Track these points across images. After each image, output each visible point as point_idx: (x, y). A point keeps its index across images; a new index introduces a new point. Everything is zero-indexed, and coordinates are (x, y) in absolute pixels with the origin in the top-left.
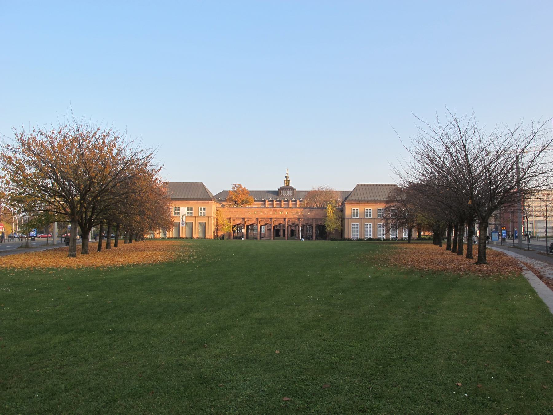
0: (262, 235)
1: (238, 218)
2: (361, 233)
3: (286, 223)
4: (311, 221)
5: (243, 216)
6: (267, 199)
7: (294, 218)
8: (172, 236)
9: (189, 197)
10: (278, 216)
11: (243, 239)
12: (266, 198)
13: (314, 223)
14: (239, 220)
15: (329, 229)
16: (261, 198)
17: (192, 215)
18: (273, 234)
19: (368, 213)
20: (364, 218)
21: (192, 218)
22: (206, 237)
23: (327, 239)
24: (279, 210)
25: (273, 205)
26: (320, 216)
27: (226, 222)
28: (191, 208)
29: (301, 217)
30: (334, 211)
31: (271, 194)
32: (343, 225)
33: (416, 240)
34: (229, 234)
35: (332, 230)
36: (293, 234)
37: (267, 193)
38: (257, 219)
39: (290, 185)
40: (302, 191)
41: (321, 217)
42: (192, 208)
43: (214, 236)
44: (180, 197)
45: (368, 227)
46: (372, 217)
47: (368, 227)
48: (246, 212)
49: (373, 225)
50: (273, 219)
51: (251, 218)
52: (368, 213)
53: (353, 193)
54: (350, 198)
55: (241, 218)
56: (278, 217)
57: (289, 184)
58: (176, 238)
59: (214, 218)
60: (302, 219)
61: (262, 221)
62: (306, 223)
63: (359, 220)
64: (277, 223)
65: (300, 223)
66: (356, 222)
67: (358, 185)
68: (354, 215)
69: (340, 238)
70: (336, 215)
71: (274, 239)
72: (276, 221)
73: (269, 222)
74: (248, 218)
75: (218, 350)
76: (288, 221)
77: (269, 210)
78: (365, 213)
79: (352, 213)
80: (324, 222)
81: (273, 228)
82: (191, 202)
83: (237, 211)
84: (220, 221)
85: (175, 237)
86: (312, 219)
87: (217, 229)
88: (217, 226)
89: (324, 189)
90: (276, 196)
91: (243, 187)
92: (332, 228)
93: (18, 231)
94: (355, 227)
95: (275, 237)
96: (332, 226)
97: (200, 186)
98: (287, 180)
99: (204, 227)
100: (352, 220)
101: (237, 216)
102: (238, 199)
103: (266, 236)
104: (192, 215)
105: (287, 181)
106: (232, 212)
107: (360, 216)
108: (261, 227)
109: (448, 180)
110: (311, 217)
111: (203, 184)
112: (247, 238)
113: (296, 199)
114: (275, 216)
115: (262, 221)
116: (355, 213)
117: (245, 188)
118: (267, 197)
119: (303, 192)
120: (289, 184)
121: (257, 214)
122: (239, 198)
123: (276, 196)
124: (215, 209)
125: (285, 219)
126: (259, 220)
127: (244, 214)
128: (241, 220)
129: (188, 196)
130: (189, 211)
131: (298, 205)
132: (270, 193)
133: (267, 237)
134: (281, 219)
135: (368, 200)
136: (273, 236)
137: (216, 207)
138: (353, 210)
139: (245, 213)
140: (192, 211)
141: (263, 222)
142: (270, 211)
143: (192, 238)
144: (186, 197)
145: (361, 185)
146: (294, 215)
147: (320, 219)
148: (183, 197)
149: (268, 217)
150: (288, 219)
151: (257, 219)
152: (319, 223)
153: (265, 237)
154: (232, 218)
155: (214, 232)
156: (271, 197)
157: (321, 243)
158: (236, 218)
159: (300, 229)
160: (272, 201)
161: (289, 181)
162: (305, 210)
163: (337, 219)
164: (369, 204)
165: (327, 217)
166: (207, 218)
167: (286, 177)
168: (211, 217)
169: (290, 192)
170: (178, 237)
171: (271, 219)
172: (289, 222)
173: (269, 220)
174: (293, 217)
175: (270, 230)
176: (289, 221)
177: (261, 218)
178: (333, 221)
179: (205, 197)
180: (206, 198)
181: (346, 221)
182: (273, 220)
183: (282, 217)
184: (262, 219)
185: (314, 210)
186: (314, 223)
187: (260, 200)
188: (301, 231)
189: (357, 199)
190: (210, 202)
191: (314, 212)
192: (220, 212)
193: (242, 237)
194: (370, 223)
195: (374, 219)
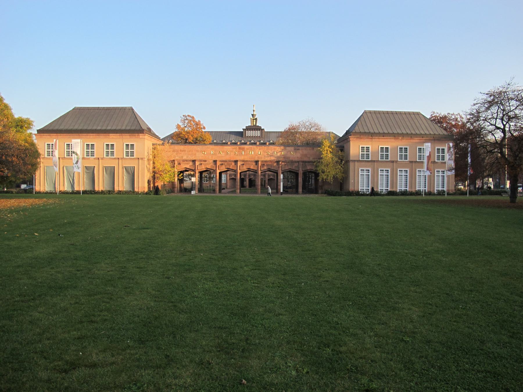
0: (223, 186)
1: (186, 161)
2: (373, 182)
3: (258, 168)
4: (296, 164)
6: (229, 141)
7: (271, 161)
8: (403, 189)
9: (109, 128)
10: (246, 158)
11: (193, 192)
12: (228, 140)
13: (301, 169)
14: (187, 164)
15: (325, 177)
16: (221, 140)
17: (133, 156)
18: (239, 184)
20: (378, 161)
21: (114, 161)
22: (136, 190)
23: (320, 191)
24: (247, 149)
26: (309, 158)
27: (168, 167)
29: (281, 159)
30: (332, 149)
31: (235, 135)
32: (346, 172)
34: (173, 183)
35: (330, 179)
36: (273, 182)
37: (229, 135)
38: (215, 162)
40: (272, 132)
41: (311, 159)
43: (149, 188)
44: (94, 128)
45: (365, 174)
46: (389, 160)
48: (198, 151)
49: (391, 172)
51: (205, 161)
52: (365, 153)
55: (190, 161)
56: (246, 160)
57: (256, 123)
58: (109, 192)
59: (148, 160)
60: (283, 162)
61: (222, 164)
62: (289, 167)
63: (370, 163)
64: (245, 168)
65: (279, 167)
66: (366, 167)
67: (365, 112)
68: (363, 155)
69: (339, 191)
70: (336, 156)
71: (240, 193)
72: (243, 164)
73: (232, 166)
74: (201, 161)
76: (262, 165)
77: (233, 149)
78: (380, 153)
79: (360, 153)
80: (316, 166)
81: (239, 175)
82: (112, 136)
83: (185, 151)
84: (158, 165)
85: (108, 189)
86: (298, 162)
87: (154, 178)
88: (154, 172)
91: (197, 120)
92: (330, 176)
95: (241, 188)
96: (329, 172)
99: (131, 173)
100: (359, 163)
101: (185, 158)
102: (188, 136)
103: (228, 187)
104: (133, 156)
105: (253, 120)
106: (177, 151)
108: (220, 174)
110: (296, 159)
111: (132, 109)
112: (201, 190)
114: (242, 158)
115: (222, 164)
116: (365, 153)
117: (199, 121)
118: (229, 139)
119: (273, 134)
120: (256, 123)
122: (190, 134)
123: (240, 138)
124: (151, 147)
125: (257, 162)
126: (218, 163)
127: (195, 154)
128: (191, 163)
129: (107, 126)
132: (233, 134)
133: (229, 189)
134: (251, 161)
135: (384, 133)
136: (239, 187)
137: (153, 145)
139: (197, 153)
140: (113, 149)
141: (224, 166)
142: (234, 150)
144: (104, 128)
145: (370, 112)
146: (271, 156)
147: (309, 162)
148: (99, 128)
149: (232, 159)
150: (262, 161)
151: (215, 162)
152: (309, 167)
153: (226, 188)
154: (177, 160)
155: (149, 182)
156: (233, 139)
158: (184, 161)
161: (256, 119)
162: (288, 148)
163: (337, 162)
164: (386, 140)
165: (322, 158)
166: (137, 161)
167: (253, 115)
168: (142, 159)
169: (258, 133)
170: (111, 189)
171: (236, 162)
172: (263, 167)
173: (233, 164)
174: (268, 159)
175: (234, 180)
176: (263, 165)
177: (221, 161)
178: (331, 165)
179: (133, 128)
181: (351, 165)
182: (239, 164)
183: (252, 160)
184: (223, 162)
185: (300, 148)
186: (301, 169)
187: (220, 142)
188: (282, 180)
189: (367, 131)
190: (141, 136)
191: (300, 151)
192: (158, 151)
193: (192, 189)
194: (387, 167)
195: (393, 162)
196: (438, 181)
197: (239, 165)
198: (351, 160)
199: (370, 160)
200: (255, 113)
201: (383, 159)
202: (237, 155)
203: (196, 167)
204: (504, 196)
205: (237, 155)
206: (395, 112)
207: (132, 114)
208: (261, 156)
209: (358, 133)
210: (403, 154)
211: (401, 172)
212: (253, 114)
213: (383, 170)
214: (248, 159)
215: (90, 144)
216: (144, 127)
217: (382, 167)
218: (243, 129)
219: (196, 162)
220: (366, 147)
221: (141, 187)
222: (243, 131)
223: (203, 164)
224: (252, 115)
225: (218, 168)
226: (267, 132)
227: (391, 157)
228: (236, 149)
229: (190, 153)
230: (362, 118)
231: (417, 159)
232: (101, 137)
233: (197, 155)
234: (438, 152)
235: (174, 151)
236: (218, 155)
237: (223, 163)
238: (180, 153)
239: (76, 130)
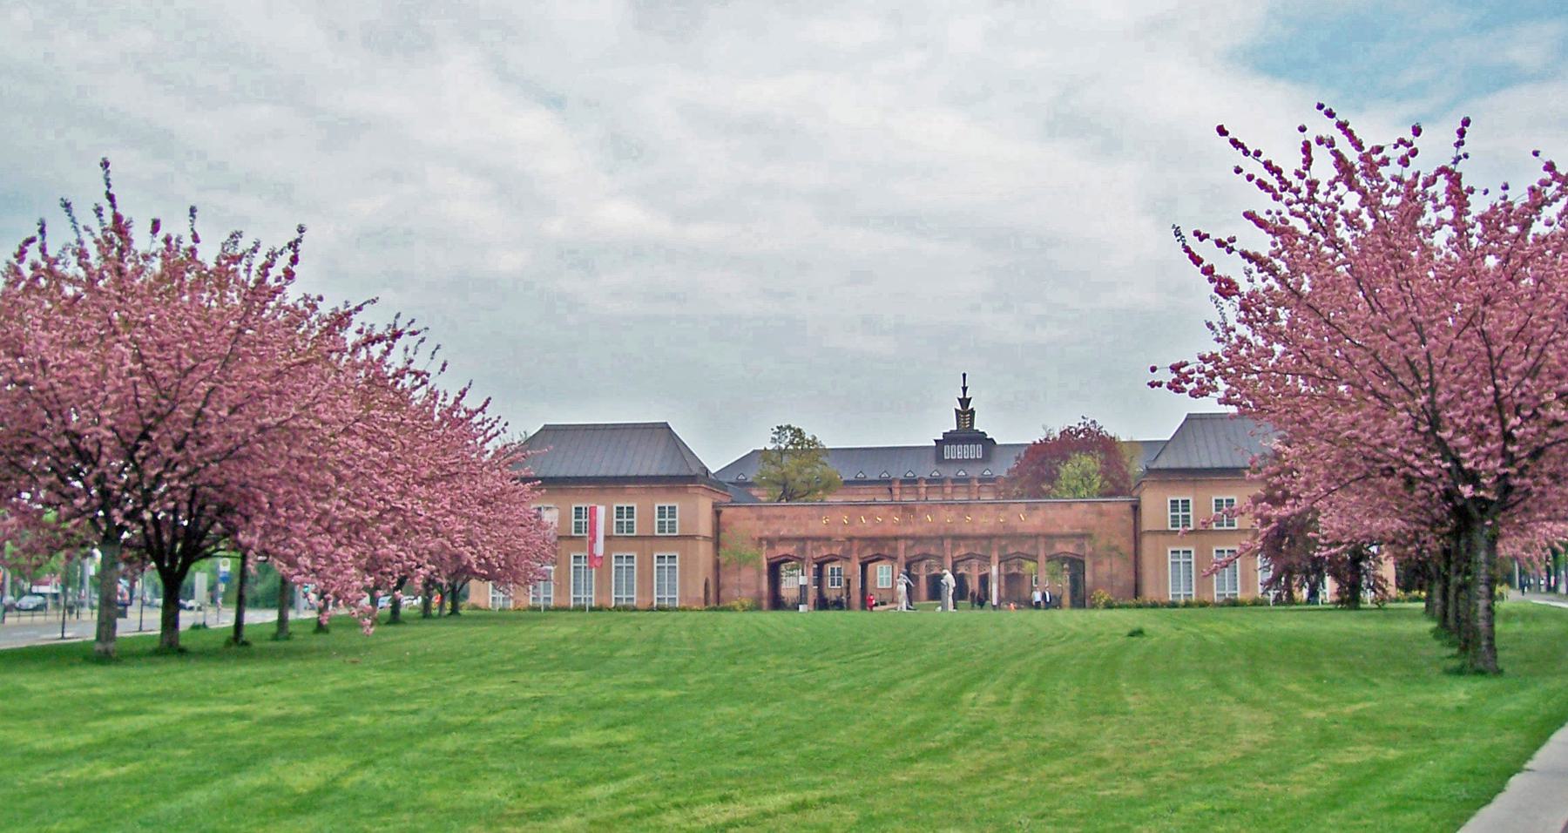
14: (790, 545)
19: (667, 520)
20: (653, 537)
28: (672, 509)
47: (1181, 560)
56: (918, 535)
63: (1193, 536)
75: (327, 687)
83: (784, 517)
93: (85, 463)
94: (1181, 560)
98: (965, 412)
107: (1239, 525)
109: (206, 531)
110: (1032, 531)
114: (909, 530)
130: (664, 517)
142: (893, 513)
157: (1078, 614)
161: (972, 412)
169: (975, 451)
180: (688, 478)
196: (591, 580)
199: (635, 534)
204: (484, 617)
210: (667, 520)
211: (1186, 554)
212: (961, 397)
213: (1178, 552)
215: (667, 505)
217: (661, 551)
218: (936, 441)
220: (1227, 501)
227: (682, 526)
232: (608, 491)
234: (661, 514)
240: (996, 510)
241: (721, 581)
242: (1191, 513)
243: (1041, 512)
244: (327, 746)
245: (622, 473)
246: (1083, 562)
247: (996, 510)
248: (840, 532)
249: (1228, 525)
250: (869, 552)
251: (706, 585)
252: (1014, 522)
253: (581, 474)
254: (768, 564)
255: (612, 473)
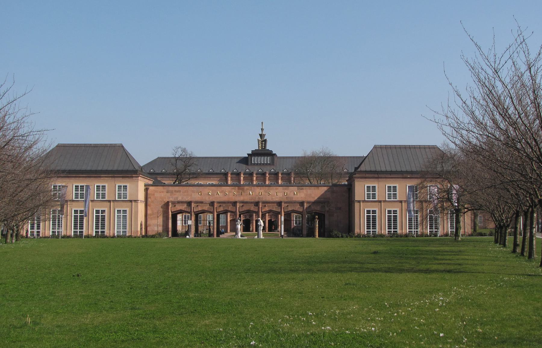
5: (188, 199)
17: (375, 198)
25: (239, 180)
33: (469, 235)
39: (268, 148)
42: (396, 187)
48: (193, 192)
50: (238, 204)
52: (79, 192)
53: (366, 159)
54: (362, 168)
56: (245, 201)
63: (377, 203)
67: (375, 147)
89: (322, 155)
90: (245, 166)
97: (119, 149)
100: (365, 203)
101: (180, 199)
104: (375, 198)
106: (172, 192)
107: (399, 198)
111: (122, 146)
112: (197, 233)
113: (277, 171)
114: (241, 198)
121: (213, 195)
123: (244, 166)
127: (191, 195)
128: (185, 205)
131: (280, 181)
138: (367, 187)
139: (193, 194)
140: (396, 191)
142: (233, 191)
143: (103, 236)
145: (381, 147)
156: (243, 168)
159: (283, 219)
160: (238, 174)
161: (265, 141)
169: (267, 159)
179: (126, 168)
181: (357, 205)
183: (252, 201)
188: (283, 223)
197: (238, 207)
198: (356, 201)
200: (264, 133)
201: (121, 198)
202: (236, 196)
203: (192, 208)
205: (236, 196)
206: (409, 147)
207: (123, 153)
208: (261, 196)
209: (363, 171)
214: (248, 200)
216: (137, 168)
217: (389, 208)
219: (193, 204)
221: (134, 231)
222: (247, 156)
223: (200, 206)
224: (260, 135)
225: (215, 210)
226: (281, 158)
228: (234, 189)
229: (186, 194)
230: (371, 153)
231: (74, 198)
233: (193, 196)
235: (167, 192)
236: (216, 196)
237: (221, 204)
238: (175, 195)
239: (91, 170)
240: (283, 189)
241: (148, 223)
242: (106, 192)
243: (304, 191)
244: (237, 291)
245: (100, 168)
246: (324, 215)
247: (283, 189)
248: (208, 199)
249: (372, 198)
250: (221, 209)
251: (141, 225)
252: (292, 195)
253: (78, 168)
254: (172, 215)
255: (94, 168)
